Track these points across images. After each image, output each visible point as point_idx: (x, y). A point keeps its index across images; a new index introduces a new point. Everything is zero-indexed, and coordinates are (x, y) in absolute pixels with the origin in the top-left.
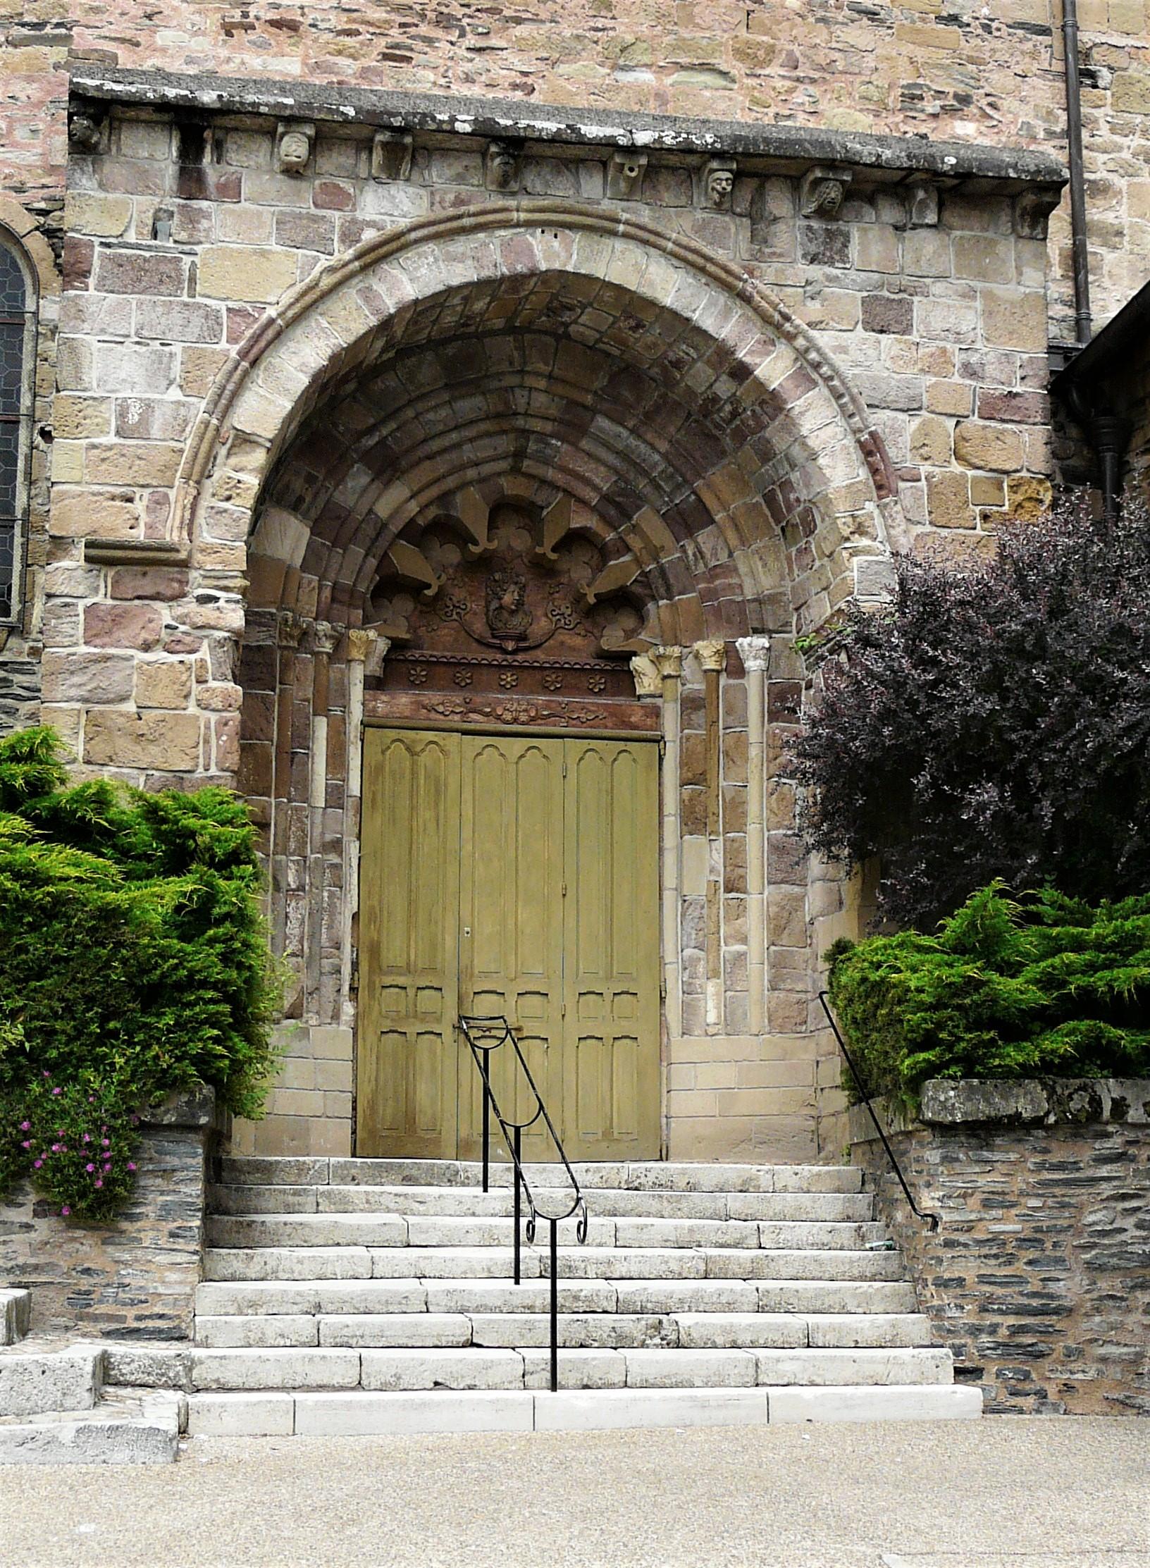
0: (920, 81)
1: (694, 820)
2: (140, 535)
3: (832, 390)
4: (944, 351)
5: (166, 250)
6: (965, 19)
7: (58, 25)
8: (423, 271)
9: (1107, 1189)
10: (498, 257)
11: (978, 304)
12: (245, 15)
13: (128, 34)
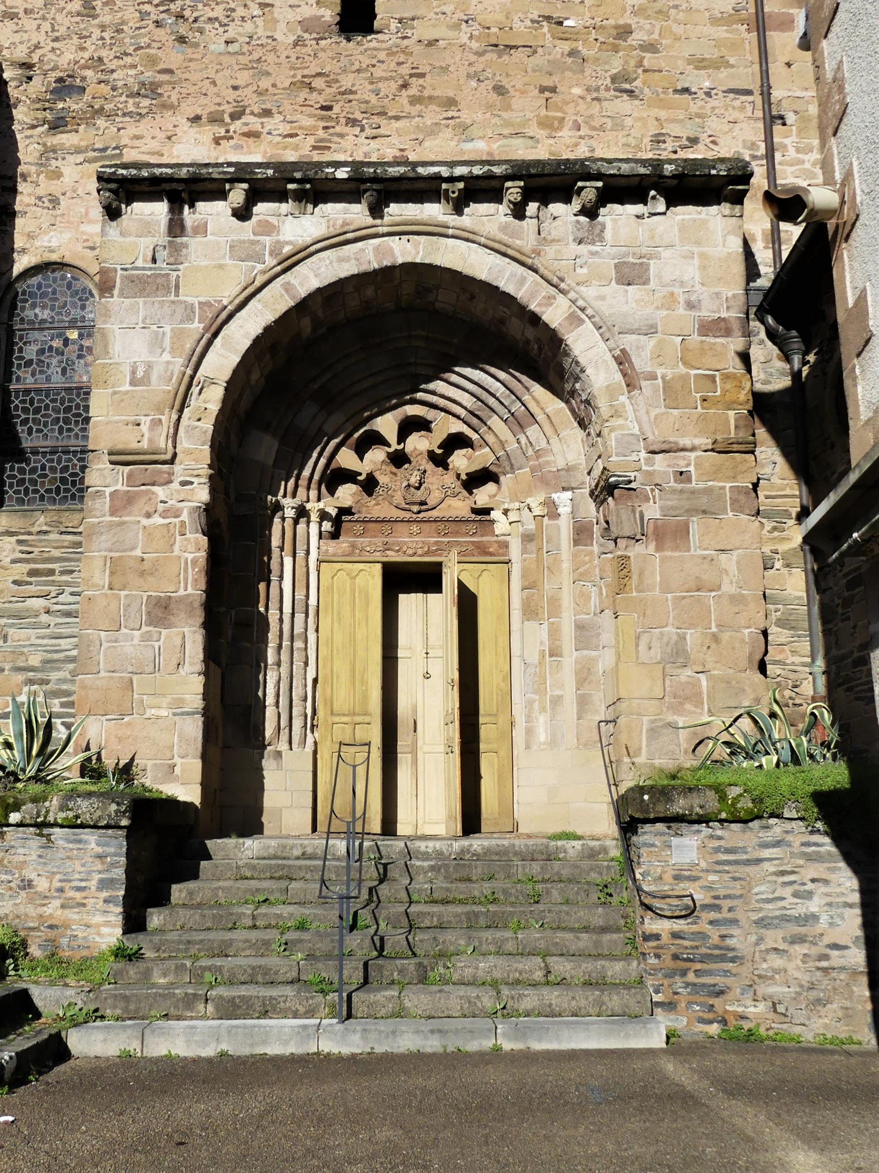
0: (664, 131)
1: (530, 612)
2: (145, 445)
3: (594, 324)
4: (672, 294)
5: (161, 269)
6: (693, 90)
7: (114, 149)
8: (323, 269)
9: (770, 867)
10: (371, 257)
11: (696, 261)
12: (228, 131)
13: (157, 149)
